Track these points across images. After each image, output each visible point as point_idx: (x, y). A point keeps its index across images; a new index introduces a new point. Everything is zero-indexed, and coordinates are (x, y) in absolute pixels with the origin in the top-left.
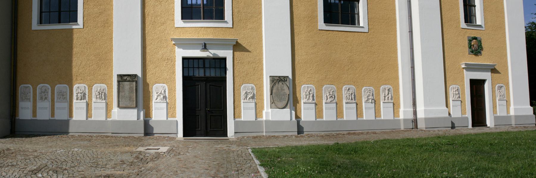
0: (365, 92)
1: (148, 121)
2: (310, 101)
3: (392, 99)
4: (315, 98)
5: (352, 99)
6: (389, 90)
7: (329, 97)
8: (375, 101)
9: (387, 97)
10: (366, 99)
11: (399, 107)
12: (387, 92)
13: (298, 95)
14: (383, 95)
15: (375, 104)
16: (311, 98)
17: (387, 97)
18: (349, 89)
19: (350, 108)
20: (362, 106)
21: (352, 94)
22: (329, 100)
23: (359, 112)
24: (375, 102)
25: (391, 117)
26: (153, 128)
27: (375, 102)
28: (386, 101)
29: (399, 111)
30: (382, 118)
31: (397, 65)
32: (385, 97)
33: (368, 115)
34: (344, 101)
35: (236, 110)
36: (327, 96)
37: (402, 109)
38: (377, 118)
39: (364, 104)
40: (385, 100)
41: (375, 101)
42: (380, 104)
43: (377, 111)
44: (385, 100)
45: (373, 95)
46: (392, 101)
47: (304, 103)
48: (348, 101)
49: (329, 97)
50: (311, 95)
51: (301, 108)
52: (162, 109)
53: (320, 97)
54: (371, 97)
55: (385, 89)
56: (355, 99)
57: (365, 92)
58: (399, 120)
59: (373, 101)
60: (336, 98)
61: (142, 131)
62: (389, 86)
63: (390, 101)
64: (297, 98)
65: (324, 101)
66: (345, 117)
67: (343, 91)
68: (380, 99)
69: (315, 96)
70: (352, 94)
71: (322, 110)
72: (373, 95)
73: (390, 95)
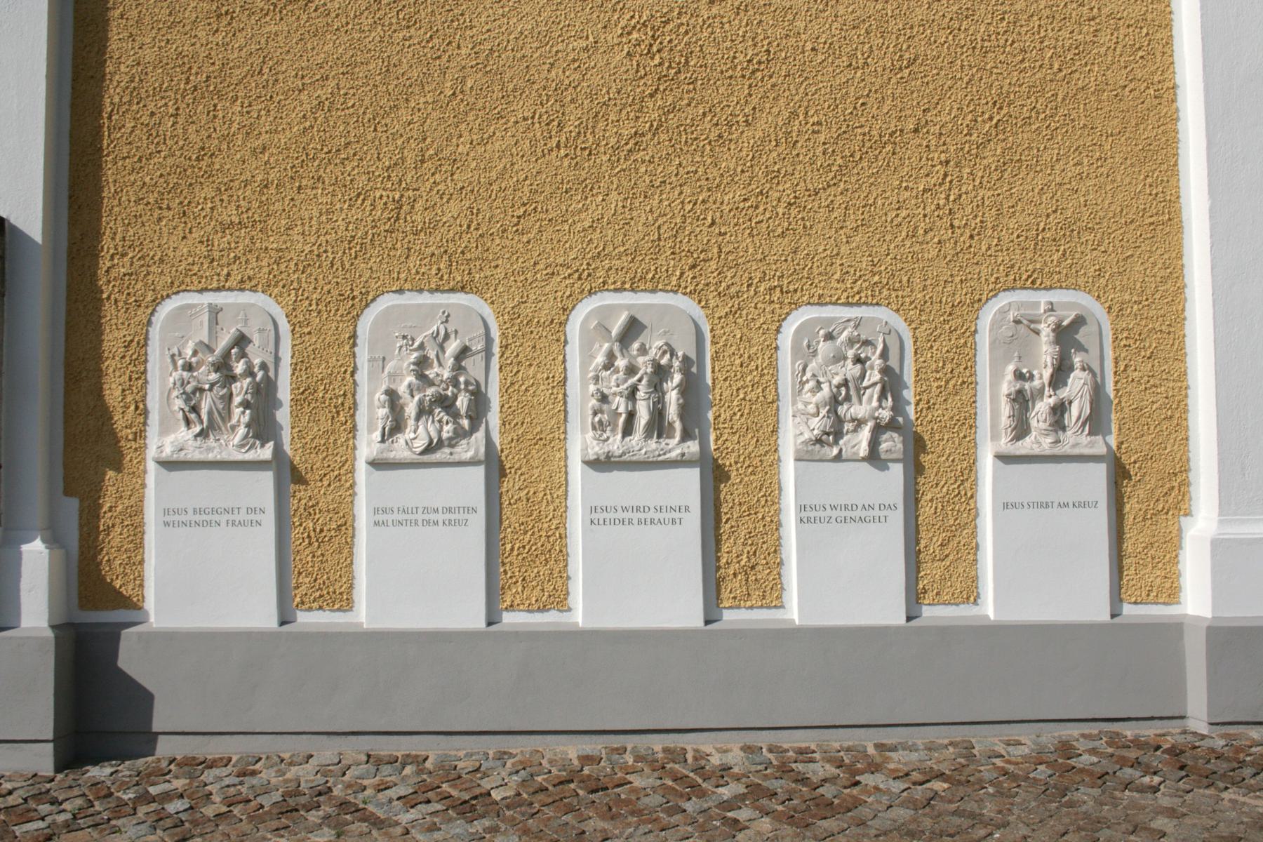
0: (805, 351)
1: (112, 635)
2: (230, 445)
3: (1095, 422)
4: (283, 416)
5: (658, 426)
6: (1066, 336)
7: (411, 409)
8: (917, 445)
9: (1042, 408)
10: (817, 425)
11: (1175, 494)
12: (1045, 353)
13: (113, 392)
14: (1007, 385)
15: (915, 469)
16: (241, 417)
17: (1042, 408)
18: (633, 328)
19: (638, 515)
20: (770, 494)
21: (660, 373)
22: (416, 436)
23: (733, 544)
24: (921, 453)
25: (1081, 598)
26: (143, 699)
27: (921, 453)
28: (1038, 441)
29: (1173, 543)
30: (989, 609)
31: (1163, 94)
32: (1021, 401)
33: (835, 567)
34: (581, 442)
35: (913, 529)
36: (392, 397)
37: (1202, 525)
38: (931, 613)
39: (789, 471)
40: (1021, 430)
41: (917, 445)
42: (968, 475)
43: (930, 541)
44: (1021, 430)
45: (891, 384)
46: (1098, 446)
47: (169, 465)
48: (616, 444)
49: (411, 409)
50: (240, 389)
51: (137, 510)
52: (669, 515)
53: (332, 403)
54: (865, 407)
55: (1029, 324)
56: (697, 418)
57: (808, 352)
58: (1174, 630)
59: (891, 443)
60: (494, 418)
61: (38, 714)
62: (1071, 301)
63: (1076, 439)
64: (104, 414)
65: (368, 445)
66: (152, 619)
67: (574, 351)
68: (968, 421)
69: (284, 393)
70: (660, 373)
71: (345, 526)
72: (891, 384)
73: (1077, 382)
